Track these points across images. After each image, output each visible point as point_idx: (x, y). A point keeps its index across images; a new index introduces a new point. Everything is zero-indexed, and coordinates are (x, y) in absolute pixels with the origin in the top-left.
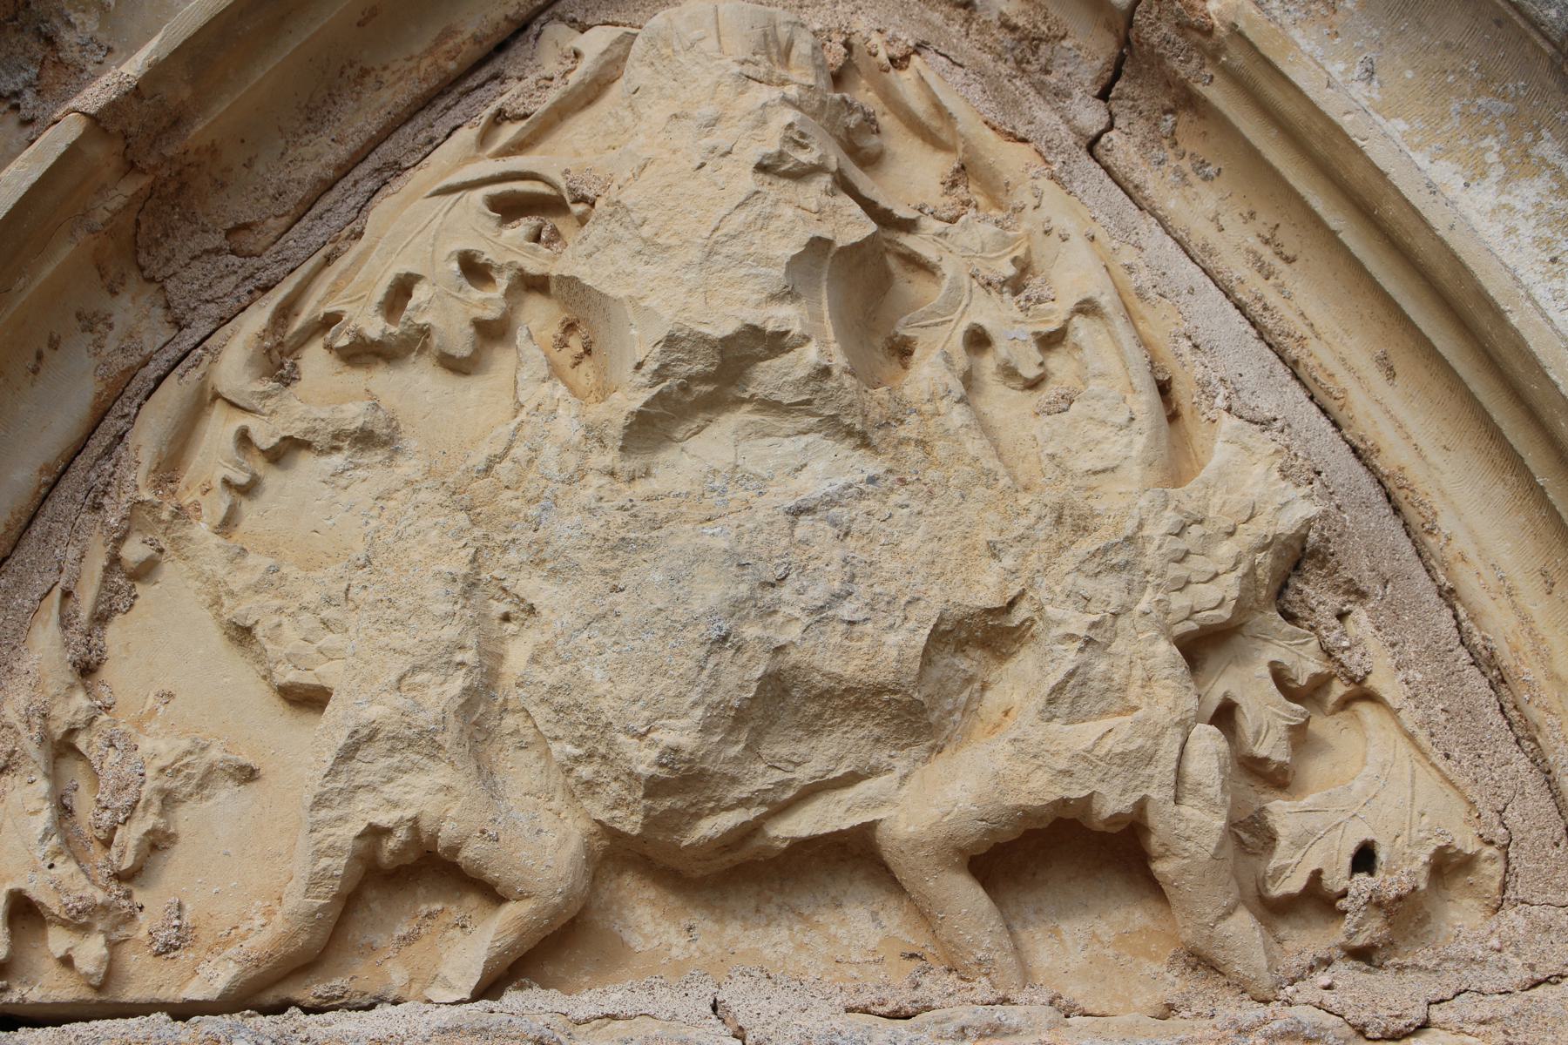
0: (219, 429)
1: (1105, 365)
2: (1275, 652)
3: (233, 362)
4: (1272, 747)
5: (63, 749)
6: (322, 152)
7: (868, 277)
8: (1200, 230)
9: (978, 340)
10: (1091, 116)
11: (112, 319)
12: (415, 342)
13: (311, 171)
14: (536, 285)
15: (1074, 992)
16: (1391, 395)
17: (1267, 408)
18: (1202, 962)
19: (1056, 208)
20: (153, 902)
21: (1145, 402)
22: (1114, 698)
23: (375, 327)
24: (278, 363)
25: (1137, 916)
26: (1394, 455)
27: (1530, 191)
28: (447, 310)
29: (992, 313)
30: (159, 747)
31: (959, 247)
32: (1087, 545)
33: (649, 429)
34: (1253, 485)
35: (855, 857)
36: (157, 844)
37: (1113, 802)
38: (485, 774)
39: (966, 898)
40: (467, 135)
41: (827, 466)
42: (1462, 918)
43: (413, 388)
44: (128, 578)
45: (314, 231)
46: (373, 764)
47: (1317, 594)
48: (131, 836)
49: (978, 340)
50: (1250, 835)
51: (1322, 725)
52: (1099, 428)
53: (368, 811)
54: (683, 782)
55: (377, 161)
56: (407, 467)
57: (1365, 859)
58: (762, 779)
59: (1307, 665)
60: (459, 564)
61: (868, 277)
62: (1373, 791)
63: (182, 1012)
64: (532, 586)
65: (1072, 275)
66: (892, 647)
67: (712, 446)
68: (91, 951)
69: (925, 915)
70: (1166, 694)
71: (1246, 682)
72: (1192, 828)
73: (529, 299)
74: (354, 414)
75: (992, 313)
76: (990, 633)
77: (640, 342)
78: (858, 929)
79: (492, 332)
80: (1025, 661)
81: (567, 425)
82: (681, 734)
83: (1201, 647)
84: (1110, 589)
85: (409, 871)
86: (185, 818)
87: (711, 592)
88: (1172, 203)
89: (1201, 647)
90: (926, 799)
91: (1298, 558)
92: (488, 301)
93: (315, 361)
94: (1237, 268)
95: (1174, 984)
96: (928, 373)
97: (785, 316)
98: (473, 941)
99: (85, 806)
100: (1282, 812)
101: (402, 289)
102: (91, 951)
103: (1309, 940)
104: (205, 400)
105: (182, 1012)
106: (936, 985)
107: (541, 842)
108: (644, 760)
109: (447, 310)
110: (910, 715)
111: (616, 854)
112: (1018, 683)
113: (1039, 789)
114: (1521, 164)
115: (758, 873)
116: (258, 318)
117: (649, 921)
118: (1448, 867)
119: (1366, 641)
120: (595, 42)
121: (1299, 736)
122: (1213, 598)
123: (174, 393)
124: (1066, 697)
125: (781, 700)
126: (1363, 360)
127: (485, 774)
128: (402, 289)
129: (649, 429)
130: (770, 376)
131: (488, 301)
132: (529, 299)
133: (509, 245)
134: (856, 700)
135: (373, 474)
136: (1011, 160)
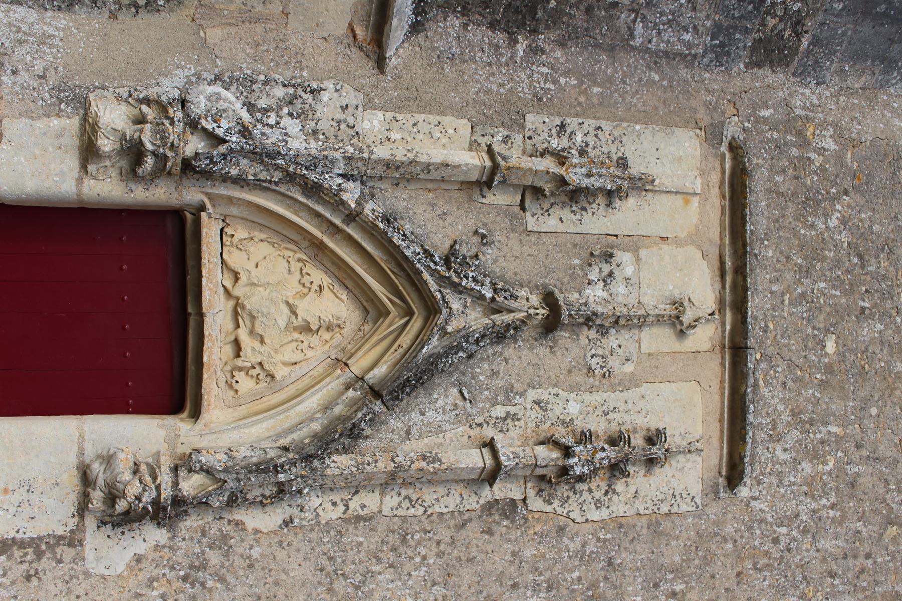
0: (291, 254)
1: (298, 356)
2: (262, 374)
3: (299, 255)
4: (250, 373)
5: (252, 239)
6: (328, 265)
7: (306, 328)
8: (316, 369)
9: (302, 342)
10: (333, 357)
11: (636, 168)
12: (303, 276)
13: (325, 263)
14: (310, 289)
15: (223, 350)
16: (294, 390)
17: (292, 375)
18: (226, 363)
19: (319, 352)
20: (234, 249)
21: (293, 361)
22: (253, 354)
23: (304, 272)
24: (299, 260)
25: (232, 357)
26: (286, 389)
27: (315, 406)
28: (307, 279)
29: (306, 344)
30: (252, 249)
31: (315, 340)
32: (272, 353)
33: (287, 303)
34: (281, 372)
35: (238, 326)
36: (241, 250)
37: (241, 354)
38: (246, 285)
39: (232, 338)
40: (330, 281)
41: (282, 323)
42: (232, 393)
43: (298, 276)
44: (273, 244)
45: (318, 264)
46: (247, 273)
47: (269, 379)
48: (241, 247)
49: (302, 342)
50: (240, 369)
51: (254, 379)
52: (289, 354)
53: (242, 273)
54: (243, 307)
55: (327, 271)
56: (287, 276)
57: (237, 382)
58: (245, 316)
59: (260, 377)
60: (271, 282)
61: (306, 328)
62: (245, 384)
63: (221, 254)
64: (268, 290)
65: (310, 353)
66: (259, 330)
67: (286, 310)
68: (228, 243)
69: (231, 333)
70: (255, 359)
71: (258, 370)
72: (239, 362)
73: (306, 287)
74: (293, 269)
75: (306, 344)
76: (262, 342)
77: (297, 303)
78: (231, 326)
79: (304, 285)
80: (259, 345)
81: (289, 294)
82: (248, 306)
83: (260, 364)
84: (266, 354)
85: (236, 277)
86: (244, 252)
87: (265, 310)
88: (320, 366)
89: (260, 364)
90: (243, 334)
91: (273, 377)
92: (308, 285)
93: (301, 264)
94: (311, 373)
95: (224, 360)
96: (296, 335)
97: (300, 319)
98: (228, 284)
99: (245, 242)
100: (242, 373)
101: (309, 275)
102: (228, 243)
103: (229, 375)
104: (295, 252)
105: (221, 254)
106: (223, 334)
107: (237, 292)
108: (245, 303)
109: (307, 279)
110: (252, 332)
111: (238, 299)
112: (257, 344)
113: (243, 346)
114: (318, 405)
115: (236, 314)
116: (305, 257)
117: (231, 303)
118: (237, 391)
119: (262, 385)
120: (344, 297)
121: (252, 376)
122: (266, 366)
123: (296, 249)
124: (253, 349)
125: (253, 318)
126: (299, 387)
127: (246, 285)
128: (309, 275)
129: (287, 303)
130: (293, 317)
131: (308, 285)
132: (306, 287)
133: (315, 287)
134: (253, 326)
135: (286, 272)
136: (327, 347)
